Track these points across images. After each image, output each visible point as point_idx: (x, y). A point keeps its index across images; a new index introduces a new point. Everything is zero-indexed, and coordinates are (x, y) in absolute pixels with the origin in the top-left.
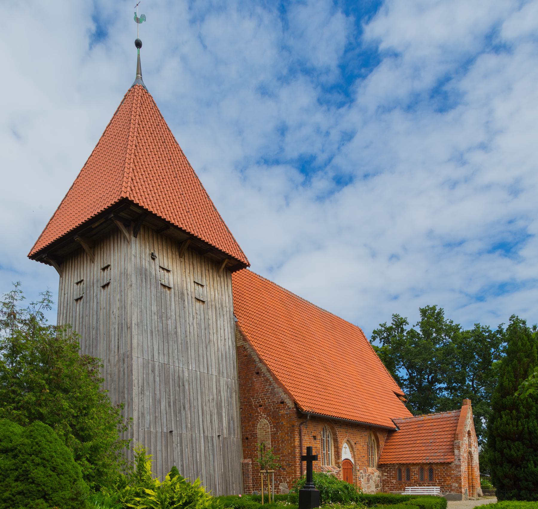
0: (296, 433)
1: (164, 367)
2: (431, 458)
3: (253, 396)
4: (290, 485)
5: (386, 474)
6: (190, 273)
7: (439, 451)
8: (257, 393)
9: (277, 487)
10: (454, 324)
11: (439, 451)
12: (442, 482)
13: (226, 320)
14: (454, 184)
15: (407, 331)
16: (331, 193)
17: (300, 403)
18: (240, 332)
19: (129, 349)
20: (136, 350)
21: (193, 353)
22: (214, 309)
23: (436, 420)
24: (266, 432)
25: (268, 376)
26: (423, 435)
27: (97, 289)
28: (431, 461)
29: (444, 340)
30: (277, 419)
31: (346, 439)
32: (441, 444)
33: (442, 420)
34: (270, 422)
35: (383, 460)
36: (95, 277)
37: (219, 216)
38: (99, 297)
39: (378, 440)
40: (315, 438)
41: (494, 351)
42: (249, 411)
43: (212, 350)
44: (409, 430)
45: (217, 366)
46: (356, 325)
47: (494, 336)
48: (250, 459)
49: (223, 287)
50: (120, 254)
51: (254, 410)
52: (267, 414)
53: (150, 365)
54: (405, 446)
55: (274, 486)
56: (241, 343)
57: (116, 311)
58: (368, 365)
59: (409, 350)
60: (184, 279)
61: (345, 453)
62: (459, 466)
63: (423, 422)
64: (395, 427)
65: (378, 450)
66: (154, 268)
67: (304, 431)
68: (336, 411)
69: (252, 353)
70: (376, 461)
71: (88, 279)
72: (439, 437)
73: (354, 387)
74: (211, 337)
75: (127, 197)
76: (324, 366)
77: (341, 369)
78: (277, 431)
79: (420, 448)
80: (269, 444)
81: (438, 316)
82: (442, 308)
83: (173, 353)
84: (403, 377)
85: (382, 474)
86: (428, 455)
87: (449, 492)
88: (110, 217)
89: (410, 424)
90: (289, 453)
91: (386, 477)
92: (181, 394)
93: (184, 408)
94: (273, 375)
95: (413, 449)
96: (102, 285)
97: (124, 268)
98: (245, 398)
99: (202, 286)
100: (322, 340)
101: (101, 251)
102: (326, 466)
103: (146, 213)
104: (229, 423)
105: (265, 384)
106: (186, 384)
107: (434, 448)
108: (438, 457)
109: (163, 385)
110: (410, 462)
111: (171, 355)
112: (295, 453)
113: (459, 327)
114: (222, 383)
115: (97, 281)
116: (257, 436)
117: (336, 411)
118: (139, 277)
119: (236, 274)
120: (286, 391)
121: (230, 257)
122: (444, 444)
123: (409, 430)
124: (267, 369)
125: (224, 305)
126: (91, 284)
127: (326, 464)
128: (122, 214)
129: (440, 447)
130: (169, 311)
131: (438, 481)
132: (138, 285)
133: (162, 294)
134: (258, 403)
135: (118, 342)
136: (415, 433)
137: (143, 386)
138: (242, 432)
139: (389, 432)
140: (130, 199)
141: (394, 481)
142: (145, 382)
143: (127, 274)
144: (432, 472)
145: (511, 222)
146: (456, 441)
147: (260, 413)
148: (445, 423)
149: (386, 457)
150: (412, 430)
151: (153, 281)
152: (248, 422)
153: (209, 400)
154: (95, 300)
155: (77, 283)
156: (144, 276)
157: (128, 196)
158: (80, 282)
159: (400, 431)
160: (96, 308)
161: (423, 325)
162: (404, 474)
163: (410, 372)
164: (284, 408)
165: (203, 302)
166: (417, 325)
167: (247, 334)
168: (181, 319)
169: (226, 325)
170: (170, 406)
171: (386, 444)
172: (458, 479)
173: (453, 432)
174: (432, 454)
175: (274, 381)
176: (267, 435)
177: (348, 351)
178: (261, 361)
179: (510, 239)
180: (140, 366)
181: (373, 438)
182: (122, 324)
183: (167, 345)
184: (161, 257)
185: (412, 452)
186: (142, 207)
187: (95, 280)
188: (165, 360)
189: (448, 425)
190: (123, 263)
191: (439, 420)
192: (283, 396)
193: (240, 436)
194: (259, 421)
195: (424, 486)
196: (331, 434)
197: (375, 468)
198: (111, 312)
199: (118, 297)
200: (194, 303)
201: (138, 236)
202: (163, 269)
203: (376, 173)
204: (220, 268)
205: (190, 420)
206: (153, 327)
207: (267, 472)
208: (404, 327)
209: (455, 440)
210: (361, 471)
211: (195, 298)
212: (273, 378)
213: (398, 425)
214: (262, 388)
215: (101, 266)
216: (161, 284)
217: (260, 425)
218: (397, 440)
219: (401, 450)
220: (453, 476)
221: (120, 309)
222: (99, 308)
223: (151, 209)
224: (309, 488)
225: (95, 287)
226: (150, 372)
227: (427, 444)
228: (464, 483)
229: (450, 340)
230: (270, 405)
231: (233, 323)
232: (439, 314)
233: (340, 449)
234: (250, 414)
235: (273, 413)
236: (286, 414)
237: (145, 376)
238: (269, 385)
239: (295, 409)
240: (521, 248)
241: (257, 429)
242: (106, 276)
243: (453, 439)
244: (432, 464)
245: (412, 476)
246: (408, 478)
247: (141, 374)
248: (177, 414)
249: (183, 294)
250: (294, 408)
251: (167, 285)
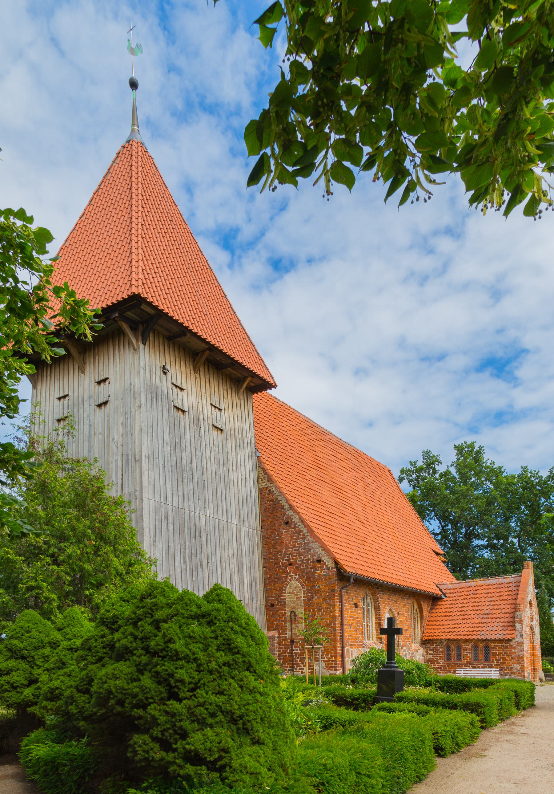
0: (337, 599)
1: (180, 511)
2: (487, 633)
3: (280, 552)
4: (328, 664)
5: (431, 652)
6: (206, 393)
7: (497, 624)
8: (286, 548)
9: (311, 666)
10: (496, 466)
11: (497, 624)
12: (501, 663)
13: (247, 455)
14: (424, 279)
15: (440, 472)
16: (270, 281)
17: (341, 561)
18: (264, 470)
19: (138, 488)
20: (147, 489)
21: (210, 495)
22: (234, 440)
23: (491, 587)
24: (297, 598)
25: (301, 526)
26: (476, 604)
27: (89, 408)
28: (487, 637)
29: (485, 486)
30: (312, 582)
31: (388, 608)
32: (498, 616)
33: (498, 586)
34: (303, 585)
35: (427, 634)
36: (87, 392)
37: (239, 321)
38: (92, 418)
39: (422, 611)
40: (356, 605)
41: (544, 502)
42: (276, 571)
43: (232, 491)
44: (458, 598)
45: (237, 512)
46: (384, 464)
47: (545, 483)
48: (276, 631)
49: (243, 413)
50: (123, 365)
51: (282, 569)
52: (299, 575)
53: (163, 510)
54: (454, 618)
55: (307, 665)
56: (265, 484)
57: (119, 438)
58: (402, 515)
59: (445, 496)
60: (200, 401)
62: (521, 644)
63: (475, 588)
64: (441, 593)
65: (421, 623)
66: (165, 385)
67: (345, 597)
68: (379, 572)
69: (280, 497)
70: (419, 636)
71: (76, 394)
72: (496, 607)
73: (391, 543)
74: (231, 475)
75: (139, 293)
76: (357, 515)
77: (374, 520)
78: (312, 596)
79: (473, 621)
80: (301, 612)
81: (477, 456)
82: (482, 446)
83: (188, 494)
84: (433, 530)
85: (427, 652)
86: (483, 629)
87: (510, 675)
88: (113, 317)
89: (459, 590)
90: (327, 625)
91: (431, 656)
92: (198, 548)
93: (201, 565)
94: (307, 526)
95: (464, 621)
96: (97, 403)
97: (129, 383)
98: (269, 553)
99: (220, 410)
100: (351, 482)
101: (94, 358)
102: (367, 641)
103: (160, 314)
104: (251, 585)
105: (296, 536)
106: (203, 534)
107: (489, 620)
108: (496, 633)
109: (177, 535)
110: (462, 637)
111: (186, 497)
112: (335, 624)
113: (502, 470)
114: (242, 534)
115: (90, 398)
116: (285, 602)
117: (379, 572)
118: (149, 396)
119: (258, 396)
120: (324, 547)
121: (254, 375)
122: (503, 616)
123: (458, 598)
124: (300, 519)
125: (245, 435)
126: (80, 401)
127: (366, 638)
128: (129, 314)
129: (498, 620)
130: (183, 440)
131: (495, 662)
132: (148, 407)
133: (176, 420)
134: (287, 560)
135: (122, 479)
136: (465, 601)
137: (155, 536)
138: (266, 597)
139: (434, 599)
140: (142, 296)
141: (441, 661)
142: (157, 531)
143: (134, 392)
144: (489, 651)
145: (500, 331)
146: (518, 613)
147: (290, 573)
148: (502, 590)
149: (432, 631)
150: (462, 598)
151: (165, 402)
152: (274, 584)
153: (229, 555)
154: (87, 422)
155: (60, 399)
156: (155, 395)
157: (140, 291)
158: (64, 397)
159: (447, 599)
160: (87, 432)
161: (461, 467)
162: (453, 653)
163: (443, 524)
164: (321, 567)
165: (222, 430)
166: (451, 466)
167: (272, 473)
168: (197, 451)
169: (247, 461)
170: (185, 562)
171: (430, 615)
172: (520, 660)
173: (513, 602)
174: (488, 629)
175: (309, 534)
176: (299, 602)
177: (378, 496)
178: (291, 507)
179: (500, 354)
180: (151, 509)
181: (416, 607)
182: (127, 455)
183: (182, 484)
184: (173, 371)
185: (464, 625)
186: (156, 308)
187: (86, 396)
188: (180, 504)
189: (506, 593)
190: (127, 376)
191: (494, 586)
192: (321, 553)
193: (263, 602)
194: (289, 583)
195: (479, 667)
196: (372, 601)
197: (418, 645)
198: (111, 439)
199: (121, 420)
200: (211, 432)
201: (147, 343)
202: (176, 386)
203: (323, 258)
204: (241, 388)
205: (207, 581)
206: (166, 461)
207: (313, 648)
208: (436, 467)
209: (516, 611)
210: (405, 648)
211: (213, 425)
212: (307, 530)
213: (444, 591)
214: (293, 542)
215: (94, 378)
216: (175, 406)
217: (290, 588)
218: (444, 610)
219: (449, 622)
220: (514, 656)
221: (124, 436)
222: (93, 433)
223: (166, 311)
224: (392, 667)
225: (86, 405)
226: (163, 517)
227: (482, 616)
228: (527, 664)
229: (492, 486)
230: (303, 564)
231: (254, 458)
232: (478, 453)
233: (382, 620)
234: (277, 574)
235: (307, 574)
237: (157, 523)
238: (302, 538)
239: (335, 570)
240: (517, 368)
241: (285, 593)
242: (103, 392)
243: (512, 610)
244: (488, 640)
245: (464, 655)
246: (459, 657)
247: (152, 521)
248: (194, 572)
249: (198, 419)
250: (334, 568)
251: (181, 407)
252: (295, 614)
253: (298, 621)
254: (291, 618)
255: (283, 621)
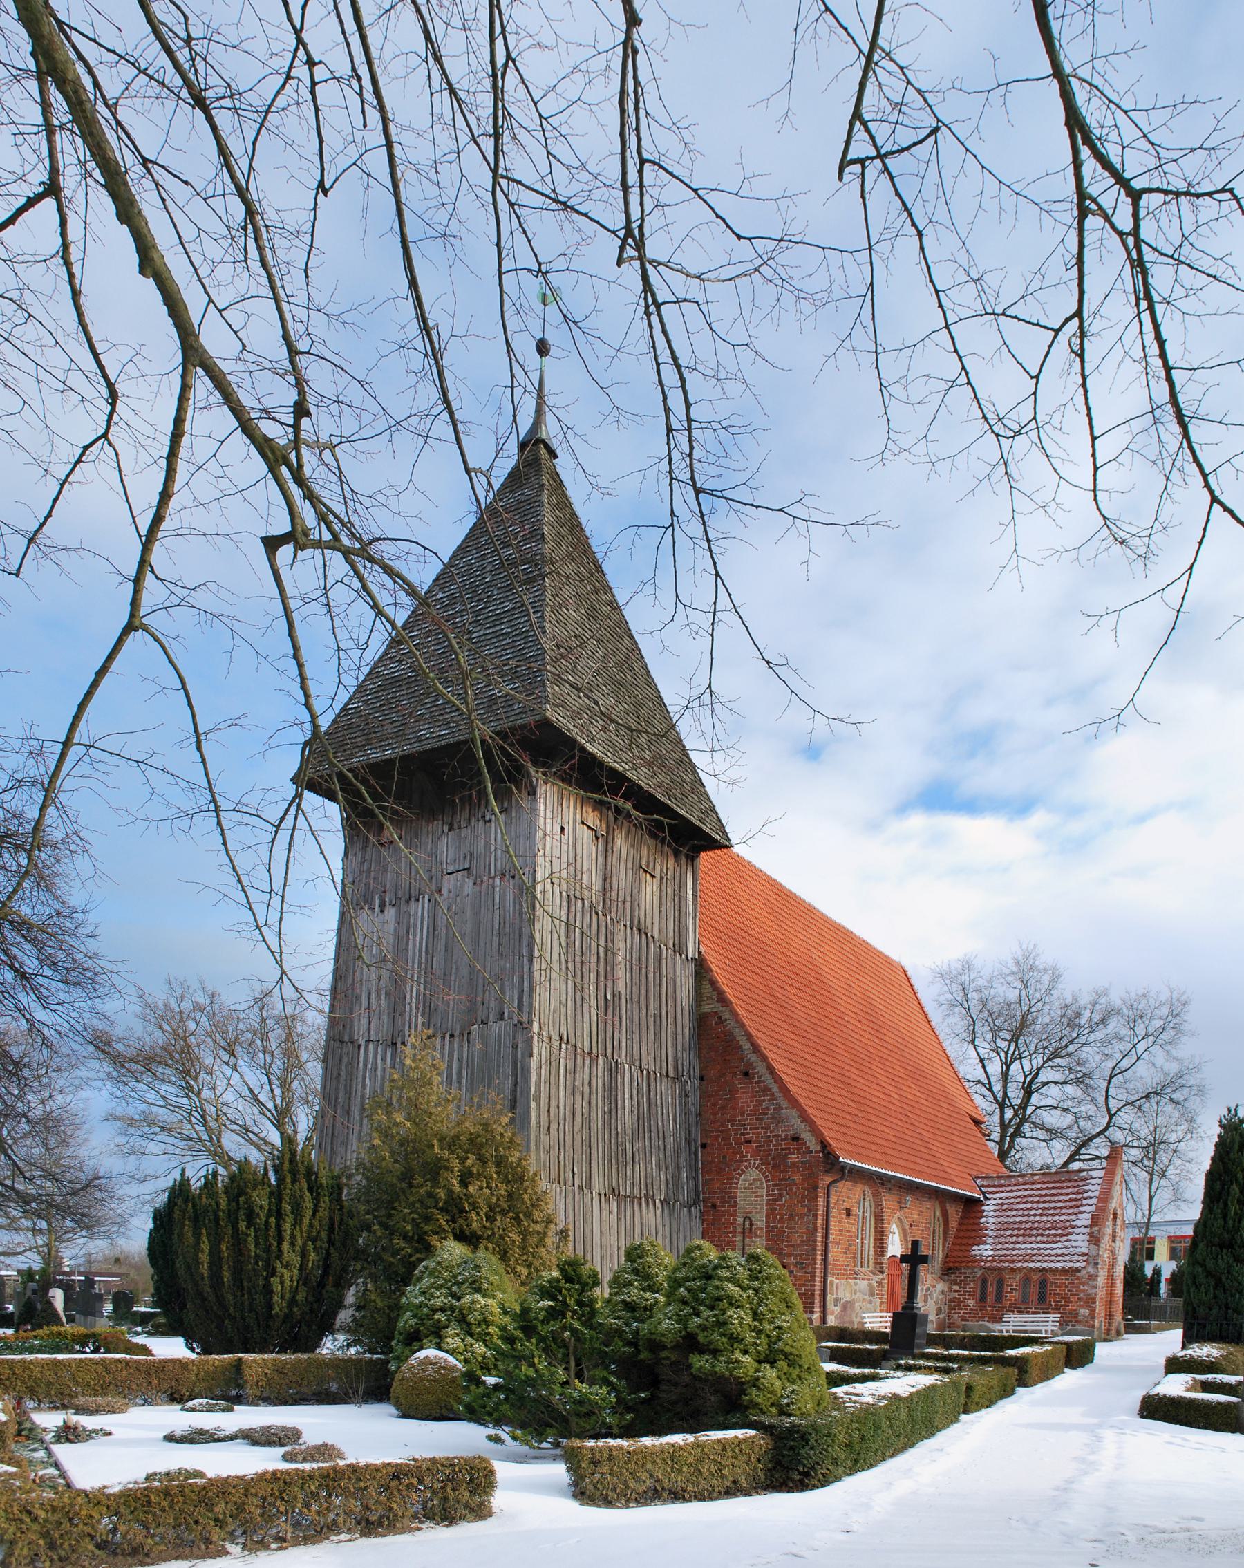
8: (742, 1115)
30: (782, 1172)
46: (897, 960)
61: (893, 1244)
80: (760, 1220)
91: (956, 1295)
116: (736, 1202)
120: (805, 1117)
134: (742, 1134)
141: (971, 1303)
172: (1090, 1301)
178: (756, 1049)
195: (1028, 1312)
228: (1100, 1309)
236: (802, 1162)
241: (736, 1188)
252: (751, 1221)
253: (756, 1233)
254: (744, 1229)
255: (730, 1232)
